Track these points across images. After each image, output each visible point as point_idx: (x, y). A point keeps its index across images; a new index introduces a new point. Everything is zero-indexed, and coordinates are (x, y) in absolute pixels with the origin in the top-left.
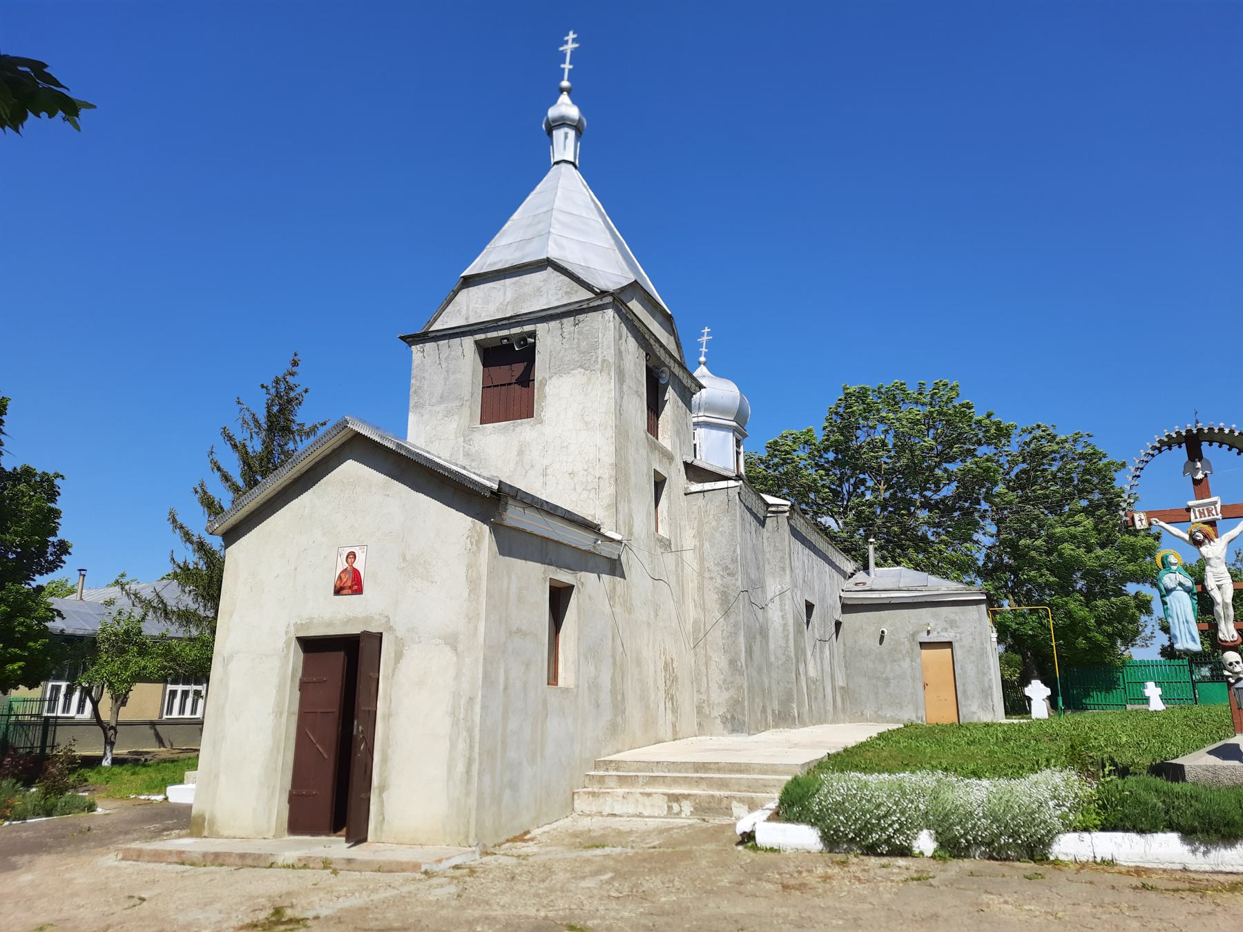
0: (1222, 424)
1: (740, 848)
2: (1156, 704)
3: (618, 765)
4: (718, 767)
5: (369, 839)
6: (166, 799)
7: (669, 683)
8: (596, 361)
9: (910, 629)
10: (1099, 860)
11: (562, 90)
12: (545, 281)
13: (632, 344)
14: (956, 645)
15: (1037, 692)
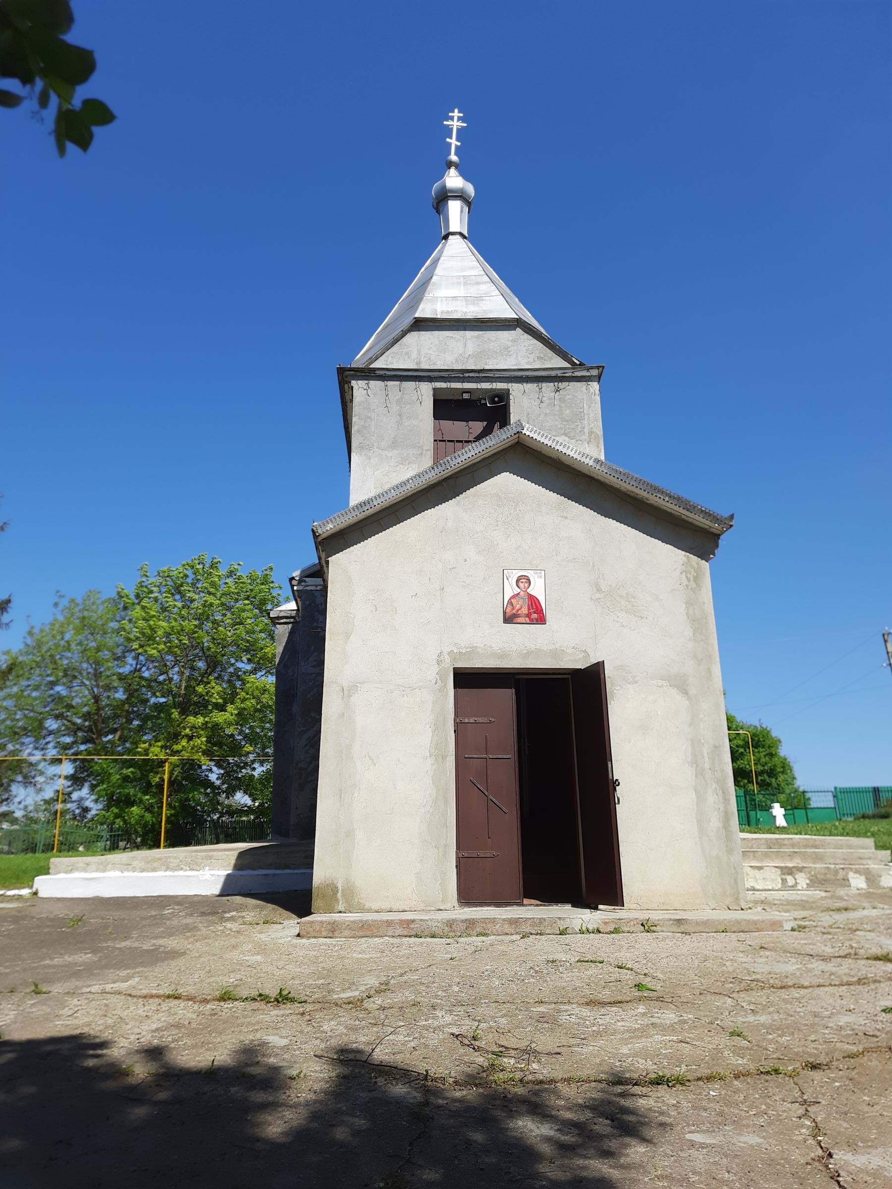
6: (36, 893)
11: (450, 164)
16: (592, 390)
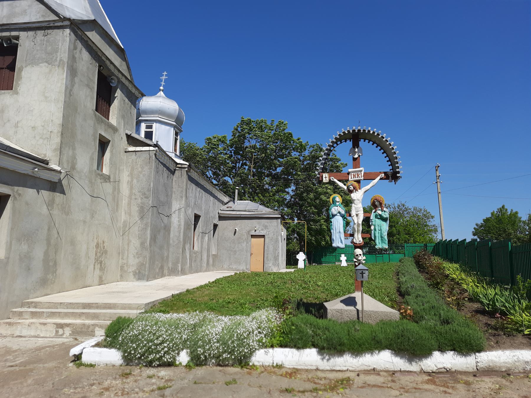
0: (370, 128)
1: (71, 365)
2: (344, 264)
3: (36, 305)
4: (97, 306)
5: (495, 208)
7: (99, 254)
8: (56, 60)
9: (248, 229)
10: (275, 365)
12: (29, 6)
13: (86, 55)
14: (266, 237)
15: (301, 257)
16: (65, 34)
